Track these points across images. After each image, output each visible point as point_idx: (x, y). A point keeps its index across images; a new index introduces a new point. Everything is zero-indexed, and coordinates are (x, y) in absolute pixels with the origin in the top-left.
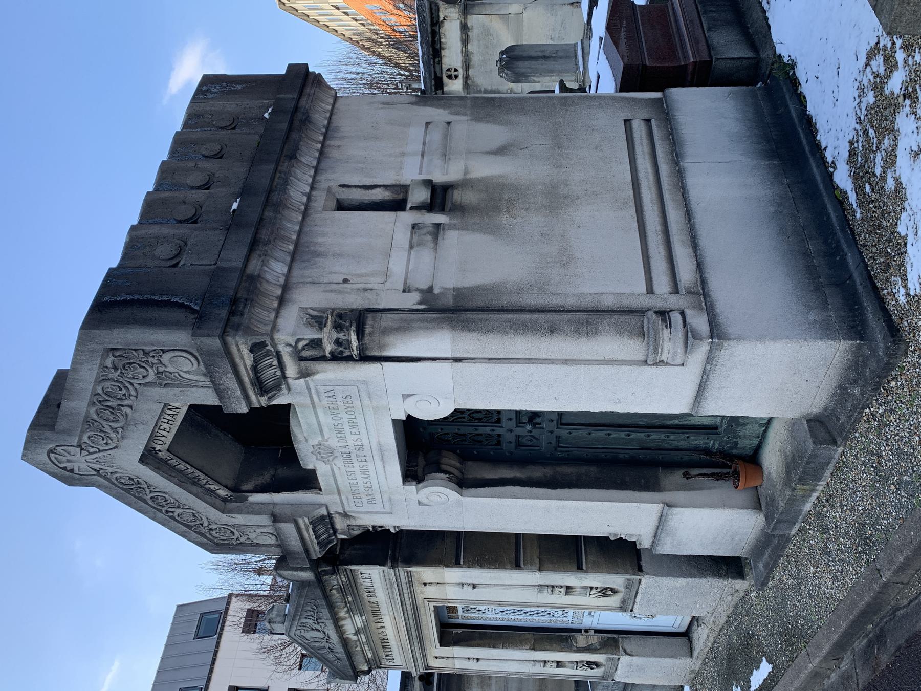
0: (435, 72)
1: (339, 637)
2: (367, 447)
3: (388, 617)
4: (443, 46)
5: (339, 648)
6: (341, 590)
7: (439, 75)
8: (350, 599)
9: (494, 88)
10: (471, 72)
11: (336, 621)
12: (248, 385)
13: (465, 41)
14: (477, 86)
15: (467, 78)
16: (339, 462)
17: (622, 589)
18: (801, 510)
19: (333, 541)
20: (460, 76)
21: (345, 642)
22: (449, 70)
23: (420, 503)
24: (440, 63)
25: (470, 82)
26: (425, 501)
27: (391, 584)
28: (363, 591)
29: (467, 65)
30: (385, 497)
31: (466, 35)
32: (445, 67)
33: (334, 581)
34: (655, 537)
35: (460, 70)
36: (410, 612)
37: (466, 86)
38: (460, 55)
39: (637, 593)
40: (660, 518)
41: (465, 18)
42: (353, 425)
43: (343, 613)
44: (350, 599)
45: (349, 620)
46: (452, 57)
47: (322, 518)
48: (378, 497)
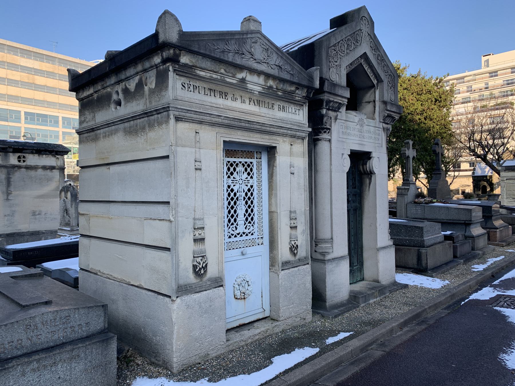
0: (27, 149)
1: (257, 70)
2: (363, 140)
3: (258, 110)
4: (41, 156)
5: (238, 60)
6: (292, 93)
7: (24, 151)
8: (280, 93)
9: (12, 183)
10: (23, 170)
11: (268, 76)
12: (392, 113)
13: (44, 168)
14: (13, 173)
15: (20, 167)
16: (358, 127)
17: (298, 257)
18: (369, 300)
19: (326, 106)
20: (20, 164)
21: (241, 68)
22: (24, 157)
23: (343, 154)
24: (32, 153)
25: (16, 168)
26: (344, 157)
27: (299, 126)
28: (286, 105)
29: (28, 168)
30: (344, 140)
31: (48, 169)
32: (27, 155)
33: (301, 93)
34: (333, 259)
35: (24, 164)
36: (268, 129)
37: (14, 167)
38: (35, 164)
39: (297, 267)
40: (342, 257)
41: (58, 169)
42: (371, 137)
43: (271, 83)
44: (280, 93)
45: (263, 83)
46: (32, 160)
47: (339, 108)
48: (345, 137)
